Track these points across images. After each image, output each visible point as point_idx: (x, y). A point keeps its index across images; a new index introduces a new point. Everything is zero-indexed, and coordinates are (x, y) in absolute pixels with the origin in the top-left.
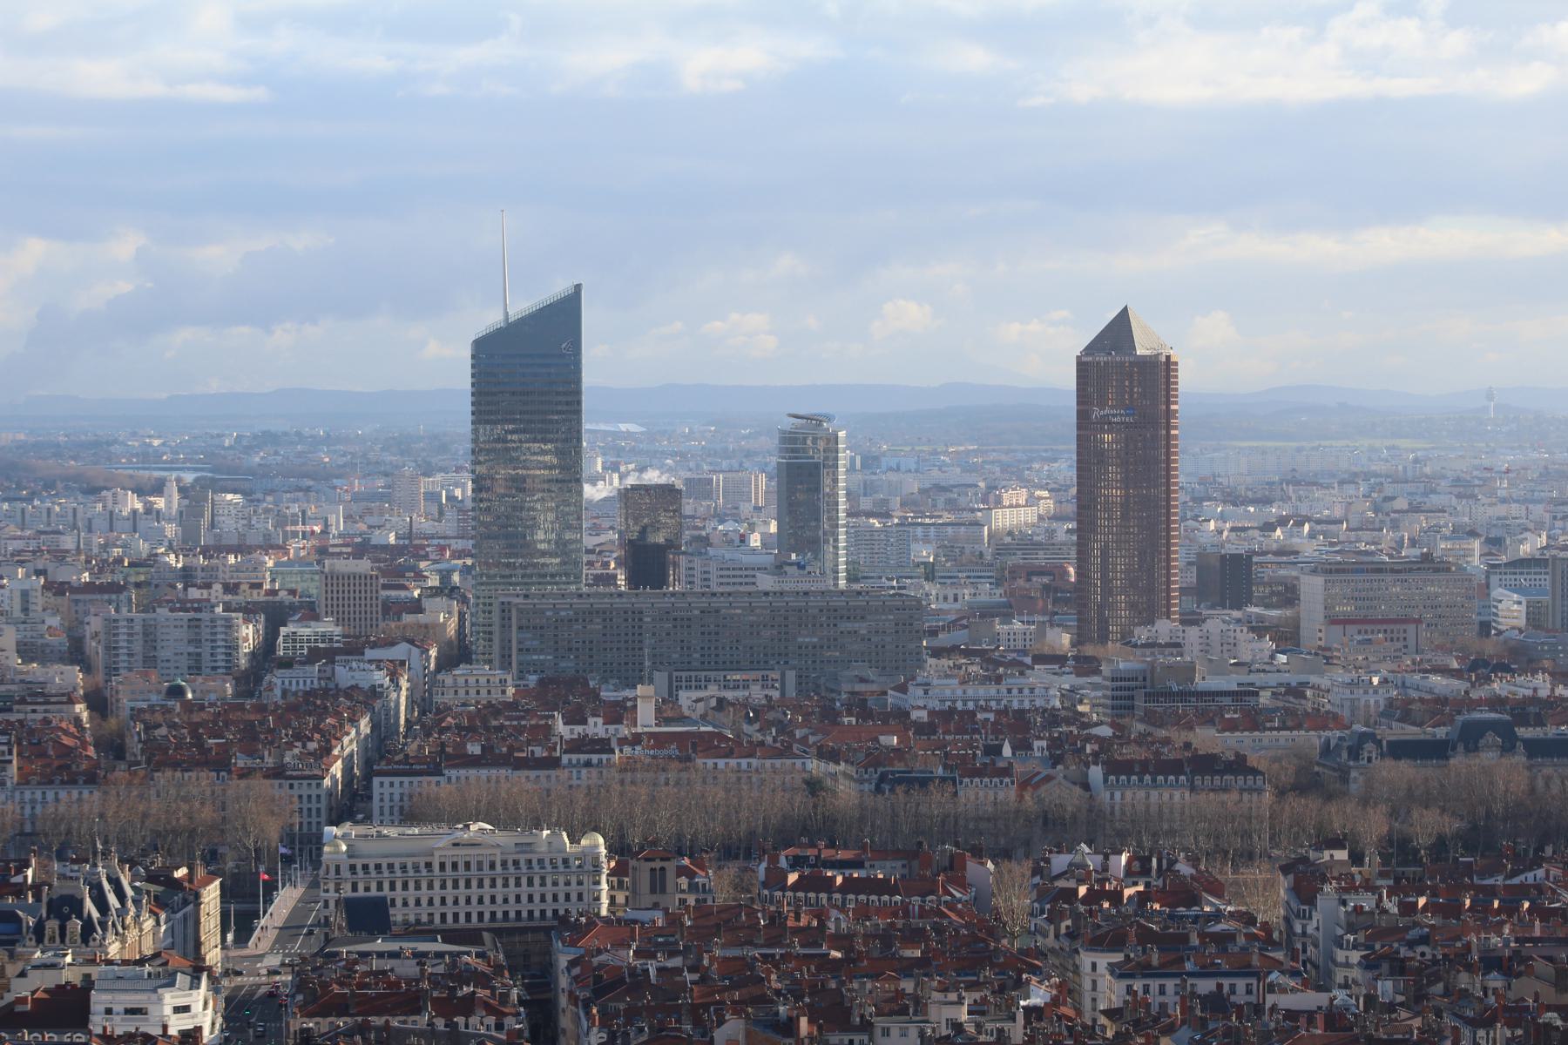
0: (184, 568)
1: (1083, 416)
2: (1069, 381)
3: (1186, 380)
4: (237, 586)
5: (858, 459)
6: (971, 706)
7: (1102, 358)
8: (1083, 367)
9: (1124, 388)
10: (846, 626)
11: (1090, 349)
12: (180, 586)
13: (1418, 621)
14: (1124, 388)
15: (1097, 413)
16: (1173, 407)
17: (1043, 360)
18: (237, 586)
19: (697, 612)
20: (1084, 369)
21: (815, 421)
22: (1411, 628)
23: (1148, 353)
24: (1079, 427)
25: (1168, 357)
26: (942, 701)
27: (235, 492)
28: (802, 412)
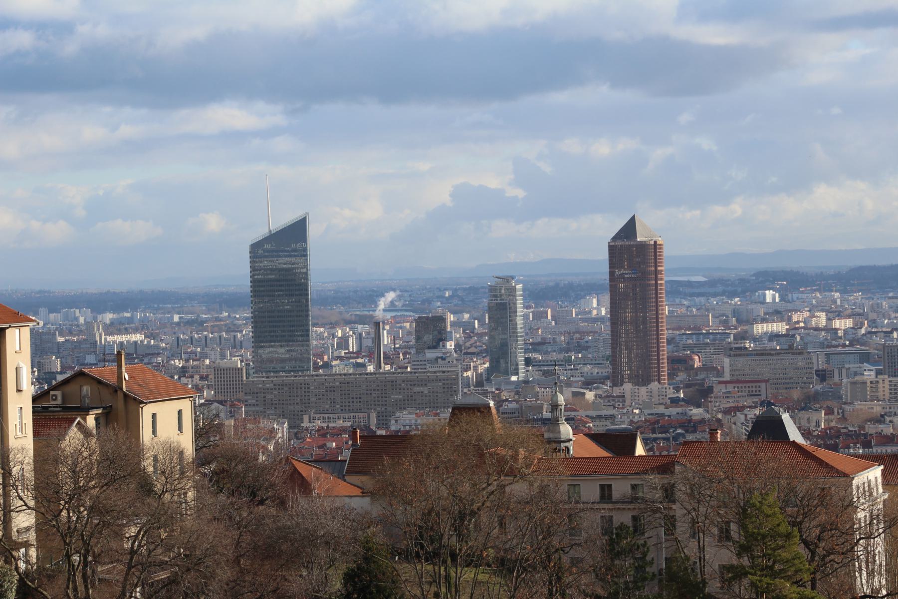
0: (183, 367)
1: (612, 274)
2: (604, 255)
3: (667, 252)
4: (207, 376)
5: (777, 295)
6: (408, 428)
7: (619, 243)
8: (612, 249)
9: (632, 257)
10: (416, 389)
11: (614, 238)
12: (176, 377)
13: (766, 381)
14: (632, 257)
15: (617, 273)
16: (659, 268)
17: (586, 245)
18: (207, 376)
19: (338, 384)
20: (613, 250)
21: (507, 279)
22: (763, 385)
23: (644, 239)
24: (611, 280)
25: (655, 242)
26: (404, 426)
27: (322, 326)
28: (501, 275)
